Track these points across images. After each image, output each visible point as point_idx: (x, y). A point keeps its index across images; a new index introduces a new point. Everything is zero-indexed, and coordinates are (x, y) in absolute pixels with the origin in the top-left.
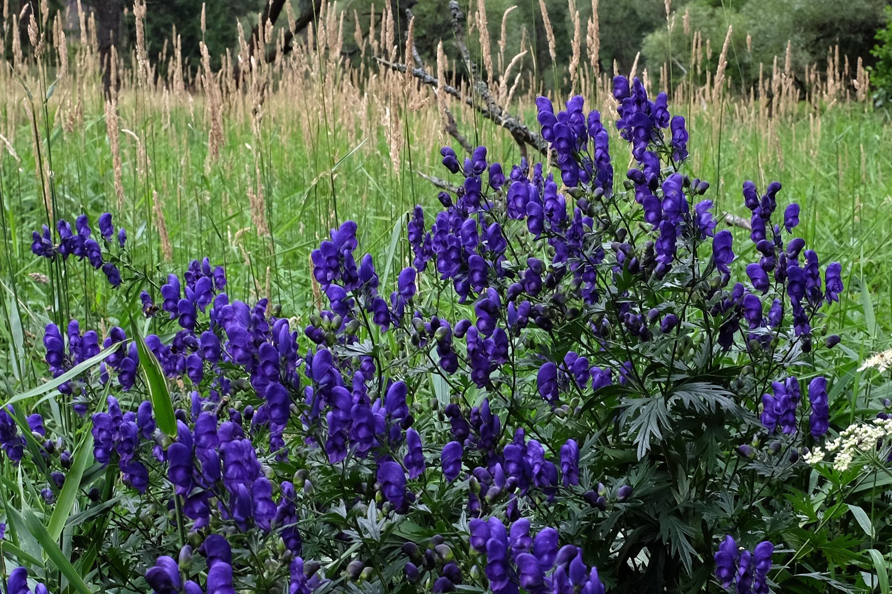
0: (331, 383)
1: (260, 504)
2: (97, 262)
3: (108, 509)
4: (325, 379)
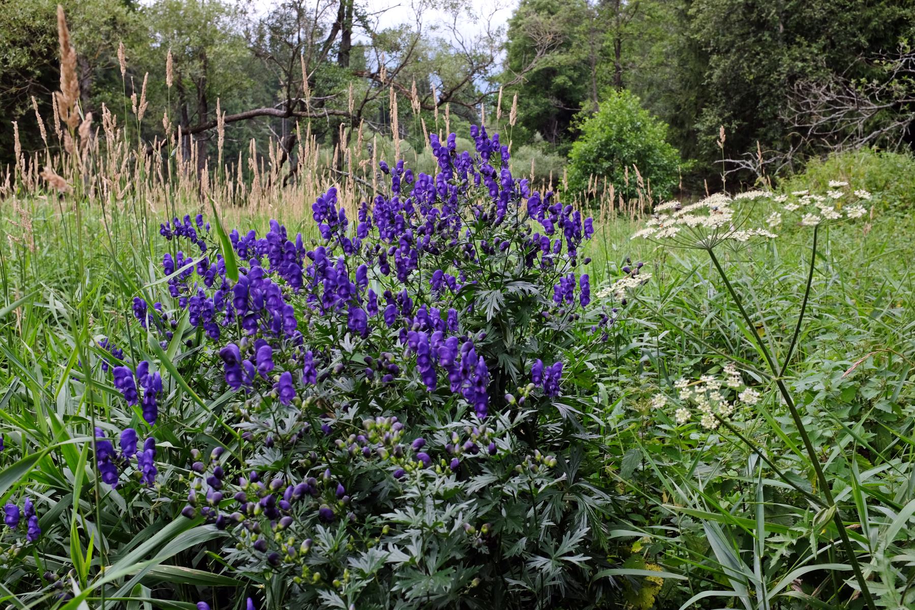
0: (325, 265)
1: (287, 320)
2: (194, 240)
3: (197, 352)
4: (322, 262)
